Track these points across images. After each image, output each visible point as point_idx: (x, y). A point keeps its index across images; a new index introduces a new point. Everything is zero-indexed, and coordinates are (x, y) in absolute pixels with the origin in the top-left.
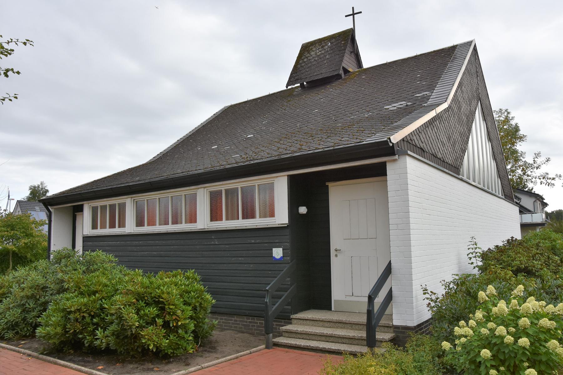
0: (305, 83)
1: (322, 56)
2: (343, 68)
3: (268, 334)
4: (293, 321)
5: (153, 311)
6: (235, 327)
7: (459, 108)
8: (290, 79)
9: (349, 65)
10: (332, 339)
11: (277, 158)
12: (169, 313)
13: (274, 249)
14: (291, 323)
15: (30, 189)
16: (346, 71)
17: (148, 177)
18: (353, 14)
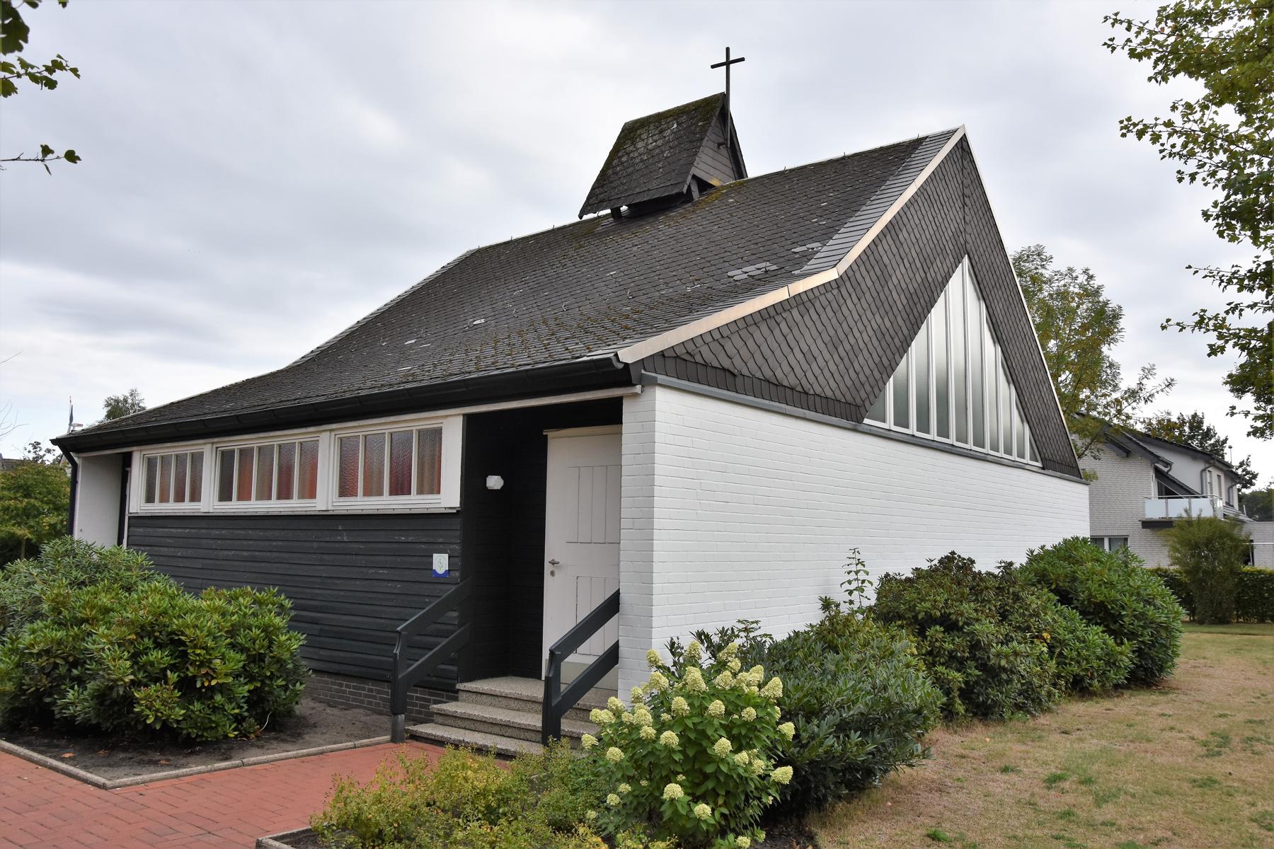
0: (624, 208)
1: (657, 151)
2: (694, 177)
3: (395, 714)
4: (462, 696)
5: (158, 657)
6: (370, 703)
7: (884, 278)
8: (589, 198)
9: (712, 171)
10: (510, 731)
11: (439, 381)
12: (193, 663)
13: (435, 556)
14: (456, 699)
15: (108, 405)
16: (704, 186)
17: (230, 408)
18: (728, 63)
